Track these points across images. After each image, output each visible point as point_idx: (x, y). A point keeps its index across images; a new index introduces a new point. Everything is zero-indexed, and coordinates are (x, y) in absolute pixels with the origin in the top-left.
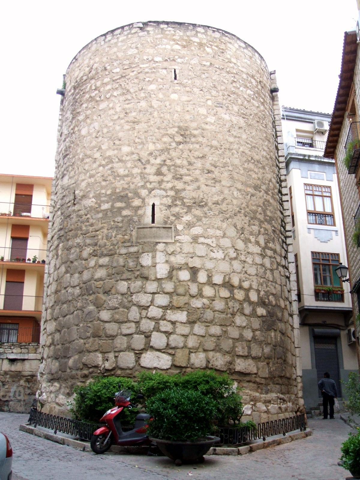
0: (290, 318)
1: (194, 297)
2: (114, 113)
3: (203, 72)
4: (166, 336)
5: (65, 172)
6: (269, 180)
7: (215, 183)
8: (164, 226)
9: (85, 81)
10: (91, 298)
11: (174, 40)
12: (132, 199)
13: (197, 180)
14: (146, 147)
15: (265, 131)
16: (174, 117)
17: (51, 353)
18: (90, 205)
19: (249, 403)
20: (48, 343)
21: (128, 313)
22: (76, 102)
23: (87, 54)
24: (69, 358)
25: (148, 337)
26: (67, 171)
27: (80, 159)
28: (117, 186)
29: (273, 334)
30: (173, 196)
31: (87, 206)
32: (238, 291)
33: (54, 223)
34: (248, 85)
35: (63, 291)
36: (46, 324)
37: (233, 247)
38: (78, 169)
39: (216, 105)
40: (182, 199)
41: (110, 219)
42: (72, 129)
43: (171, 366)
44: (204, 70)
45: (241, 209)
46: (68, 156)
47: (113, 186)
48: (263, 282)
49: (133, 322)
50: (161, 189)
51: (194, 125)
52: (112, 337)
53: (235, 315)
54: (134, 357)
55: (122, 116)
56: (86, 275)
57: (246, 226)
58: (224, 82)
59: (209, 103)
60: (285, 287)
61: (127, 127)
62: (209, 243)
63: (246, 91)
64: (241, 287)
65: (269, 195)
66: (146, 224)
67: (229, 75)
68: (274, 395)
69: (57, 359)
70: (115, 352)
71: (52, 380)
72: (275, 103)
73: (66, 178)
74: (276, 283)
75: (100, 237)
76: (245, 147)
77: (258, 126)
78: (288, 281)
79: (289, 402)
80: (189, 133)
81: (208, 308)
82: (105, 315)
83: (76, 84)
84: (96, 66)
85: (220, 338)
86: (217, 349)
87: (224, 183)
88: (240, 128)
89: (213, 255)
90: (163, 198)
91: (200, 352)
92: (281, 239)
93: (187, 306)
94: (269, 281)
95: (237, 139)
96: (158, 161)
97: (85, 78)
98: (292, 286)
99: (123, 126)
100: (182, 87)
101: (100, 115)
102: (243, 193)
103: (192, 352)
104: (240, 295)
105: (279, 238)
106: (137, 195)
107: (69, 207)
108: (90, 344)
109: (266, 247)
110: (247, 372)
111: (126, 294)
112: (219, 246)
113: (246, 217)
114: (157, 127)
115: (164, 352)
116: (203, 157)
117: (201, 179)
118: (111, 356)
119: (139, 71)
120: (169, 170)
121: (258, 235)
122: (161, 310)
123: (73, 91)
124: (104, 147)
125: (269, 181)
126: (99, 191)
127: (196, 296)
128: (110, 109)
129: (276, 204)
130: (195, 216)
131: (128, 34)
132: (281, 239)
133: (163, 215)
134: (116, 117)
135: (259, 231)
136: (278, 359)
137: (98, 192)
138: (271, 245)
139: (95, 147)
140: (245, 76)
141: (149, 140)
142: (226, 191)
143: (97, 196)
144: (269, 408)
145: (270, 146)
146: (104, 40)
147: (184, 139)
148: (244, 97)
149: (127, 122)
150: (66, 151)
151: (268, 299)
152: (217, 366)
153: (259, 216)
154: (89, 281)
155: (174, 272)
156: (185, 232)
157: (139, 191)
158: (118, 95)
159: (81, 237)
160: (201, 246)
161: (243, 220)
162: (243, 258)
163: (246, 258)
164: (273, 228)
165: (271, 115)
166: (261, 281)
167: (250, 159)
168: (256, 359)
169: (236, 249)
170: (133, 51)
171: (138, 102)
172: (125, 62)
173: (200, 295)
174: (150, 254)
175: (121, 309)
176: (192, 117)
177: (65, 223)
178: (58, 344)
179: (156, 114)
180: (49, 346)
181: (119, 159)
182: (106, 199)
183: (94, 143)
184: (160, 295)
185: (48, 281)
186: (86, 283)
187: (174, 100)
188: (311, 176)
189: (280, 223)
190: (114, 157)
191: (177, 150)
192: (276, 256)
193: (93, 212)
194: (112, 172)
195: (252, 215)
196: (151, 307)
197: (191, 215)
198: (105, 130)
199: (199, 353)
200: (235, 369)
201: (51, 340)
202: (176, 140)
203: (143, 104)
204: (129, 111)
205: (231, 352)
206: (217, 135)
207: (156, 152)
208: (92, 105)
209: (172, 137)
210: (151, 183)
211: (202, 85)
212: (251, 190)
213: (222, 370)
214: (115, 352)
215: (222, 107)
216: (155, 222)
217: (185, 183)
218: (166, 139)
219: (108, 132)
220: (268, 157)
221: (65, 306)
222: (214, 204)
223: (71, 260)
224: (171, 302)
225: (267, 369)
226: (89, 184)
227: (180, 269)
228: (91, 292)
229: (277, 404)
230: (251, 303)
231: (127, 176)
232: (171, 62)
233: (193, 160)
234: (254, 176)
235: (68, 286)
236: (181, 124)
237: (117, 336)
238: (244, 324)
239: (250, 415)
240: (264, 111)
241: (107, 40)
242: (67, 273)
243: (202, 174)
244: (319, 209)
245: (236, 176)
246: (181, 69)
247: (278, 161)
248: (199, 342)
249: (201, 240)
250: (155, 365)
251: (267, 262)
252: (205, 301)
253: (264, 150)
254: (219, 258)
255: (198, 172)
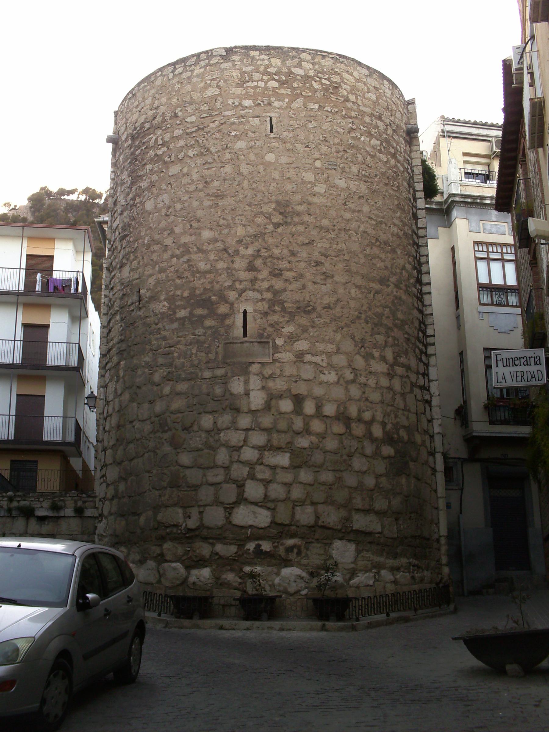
0: (431, 459)
1: (299, 434)
2: (190, 182)
3: (309, 119)
4: (264, 485)
5: (125, 261)
6: (401, 267)
7: (325, 280)
8: (259, 340)
9: (147, 130)
10: (167, 435)
11: (269, 74)
12: (216, 304)
13: (301, 276)
14: (233, 232)
15: (396, 196)
16: (270, 188)
17: (114, 509)
18: (161, 311)
19: (370, 571)
20: (109, 496)
21: (215, 456)
22: (136, 160)
23: (149, 90)
24: (139, 515)
25: (241, 486)
26: (128, 260)
27: (144, 244)
28: (197, 286)
29: (403, 481)
30: (270, 300)
31: (157, 312)
32: (356, 424)
33: (110, 331)
34: (373, 131)
35: (129, 426)
36: (105, 469)
37: (350, 365)
38: (143, 258)
39: (327, 166)
40: (282, 303)
41: (188, 331)
42: (131, 199)
43: (271, 523)
44: (311, 116)
45: (360, 313)
46: (128, 238)
47: (191, 285)
48: (391, 411)
49: (221, 467)
50: (254, 290)
51: (297, 198)
52: (196, 488)
53: (352, 456)
54: (223, 512)
55: (200, 186)
56: (159, 407)
57: (368, 337)
58: (338, 133)
59: (318, 164)
60: (423, 415)
61: (207, 203)
62: (317, 362)
63: (370, 141)
64: (360, 420)
65: (401, 289)
66: (236, 338)
67: (346, 120)
68: (404, 561)
69: (122, 516)
70: (200, 506)
71: (117, 543)
72: (414, 148)
73: (126, 269)
74: (409, 411)
75: (176, 354)
76: (367, 225)
77: (386, 191)
78: (428, 408)
79: (427, 570)
80: (291, 210)
81: (317, 448)
82: (185, 459)
83: (135, 132)
84: (162, 109)
85: (333, 487)
86: (329, 501)
87: (337, 278)
88: (360, 197)
89: (323, 378)
90: (257, 302)
91: (307, 505)
92: (419, 349)
93: (290, 446)
94: (398, 409)
95: (356, 214)
96: (250, 251)
97: (147, 125)
98: (434, 413)
99: (202, 202)
100: (280, 143)
101: (170, 184)
102: (363, 291)
103: (297, 506)
104: (358, 430)
105: (415, 348)
106: (224, 299)
107: (132, 311)
108: (167, 497)
109: (396, 363)
110: (368, 530)
111: (211, 431)
112: (331, 365)
113: (367, 323)
114: (247, 203)
115: (261, 506)
116: (309, 243)
117: (307, 275)
118: (194, 512)
119: (222, 121)
120: (265, 263)
121: (384, 348)
122: (256, 451)
123: (130, 142)
124: (177, 230)
125: (402, 269)
126: (173, 292)
127: (302, 432)
128: (184, 175)
129: (411, 300)
130: (299, 325)
131: (206, 65)
132: (419, 349)
133: (258, 326)
134: (192, 188)
135: (386, 342)
136: (411, 513)
137: (171, 294)
138: (402, 360)
139: (165, 230)
140: (367, 119)
141: (237, 221)
142: (341, 291)
143: (171, 299)
144: (398, 576)
145: (405, 218)
146: (173, 72)
147: (284, 219)
148: (367, 151)
149: (208, 195)
150: (124, 229)
151: (398, 434)
152: (329, 523)
153: (385, 321)
154: (164, 413)
155: (273, 402)
156: (287, 347)
157: (226, 293)
158: (194, 155)
159: (150, 354)
160: (307, 366)
161: (363, 328)
162: (363, 380)
163: (367, 380)
164: (406, 336)
165: (407, 169)
166: (388, 411)
167: (374, 241)
168: (380, 514)
169: (353, 369)
170: (212, 92)
171: (222, 167)
172: (202, 108)
173: (307, 431)
174: (242, 379)
175: (206, 451)
176: (294, 186)
177: (128, 333)
178: (124, 497)
179: (245, 184)
180: (112, 499)
181: (198, 248)
182: (182, 303)
183: (163, 224)
184: (255, 432)
185: (105, 412)
186: (160, 416)
187: (270, 163)
188: (484, 229)
189: (418, 327)
190: (191, 246)
191: (275, 234)
192: (409, 374)
193: (166, 320)
194: (189, 266)
195: (376, 321)
196: (244, 447)
197: (294, 324)
198: (178, 206)
199: (306, 507)
200: (352, 527)
201: (113, 491)
202: (273, 221)
203: (228, 169)
204: (210, 180)
205: (347, 505)
206: (328, 210)
207: (247, 238)
208: (158, 167)
209: (268, 217)
210: (241, 282)
211: (307, 140)
212: (376, 286)
213: (336, 528)
214: (200, 506)
215: (335, 169)
216: (248, 336)
217: (286, 280)
218: (260, 220)
219: (182, 209)
220: (401, 233)
221: (131, 446)
222: (324, 308)
223: (138, 385)
224: (269, 441)
225: (395, 527)
226: (158, 282)
227: (281, 397)
228: (167, 428)
229: (409, 572)
230: (373, 440)
231: (209, 272)
232: (266, 108)
233: (296, 249)
234: (380, 264)
235: (134, 420)
236: (280, 198)
237: (201, 485)
238: (365, 469)
239: (371, 586)
240: (396, 166)
241: (176, 72)
242: (133, 402)
243: (308, 267)
244: (497, 280)
245: (354, 268)
246: (279, 117)
247: (417, 234)
248: (306, 492)
249: (308, 358)
250: (250, 523)
251: (397, 384)
252: (313, 439)
253: (395, 225)
254: (332, 381)
255: (303, 265)
